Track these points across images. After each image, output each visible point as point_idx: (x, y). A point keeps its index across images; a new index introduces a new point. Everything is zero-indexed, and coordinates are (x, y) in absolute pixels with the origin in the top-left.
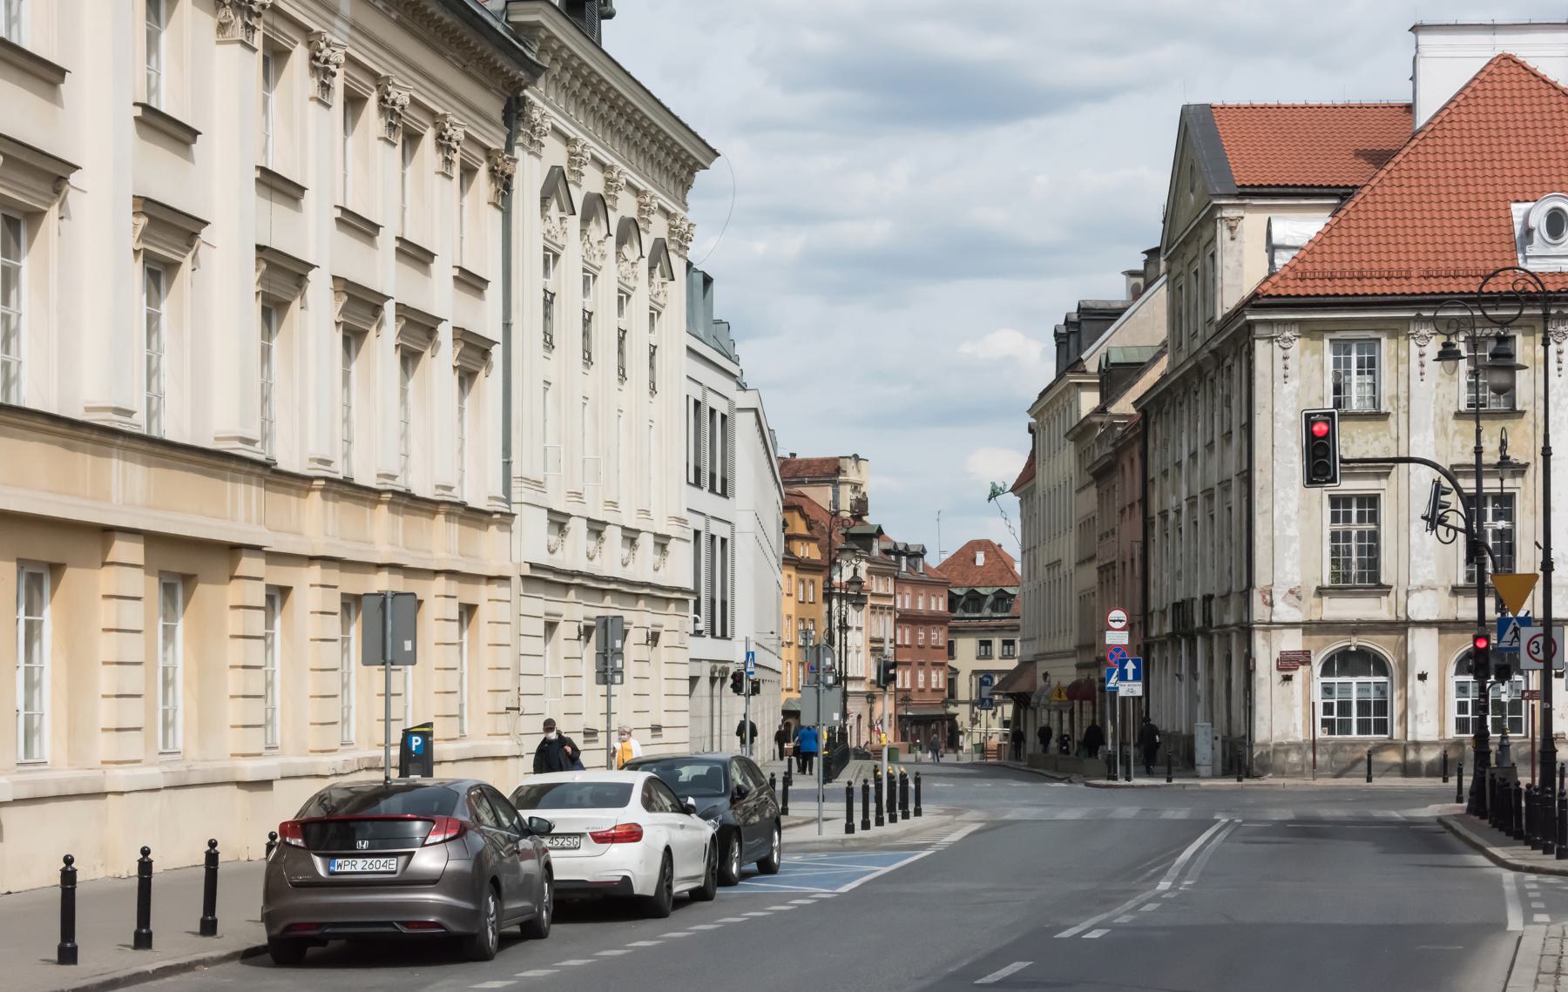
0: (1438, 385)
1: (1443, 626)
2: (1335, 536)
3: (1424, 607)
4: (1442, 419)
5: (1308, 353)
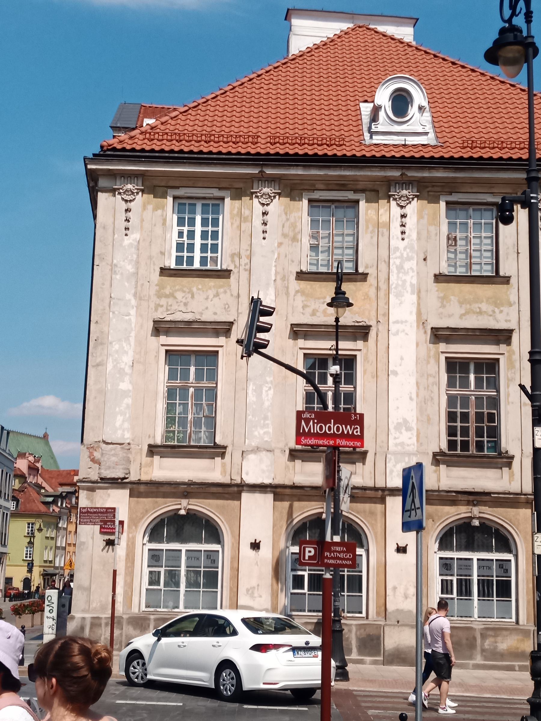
0: (280, 244)
1: (279, 492)
2: (171, 393)
3: (255, 470)
4: (284, 278)
5: (150, 207)
